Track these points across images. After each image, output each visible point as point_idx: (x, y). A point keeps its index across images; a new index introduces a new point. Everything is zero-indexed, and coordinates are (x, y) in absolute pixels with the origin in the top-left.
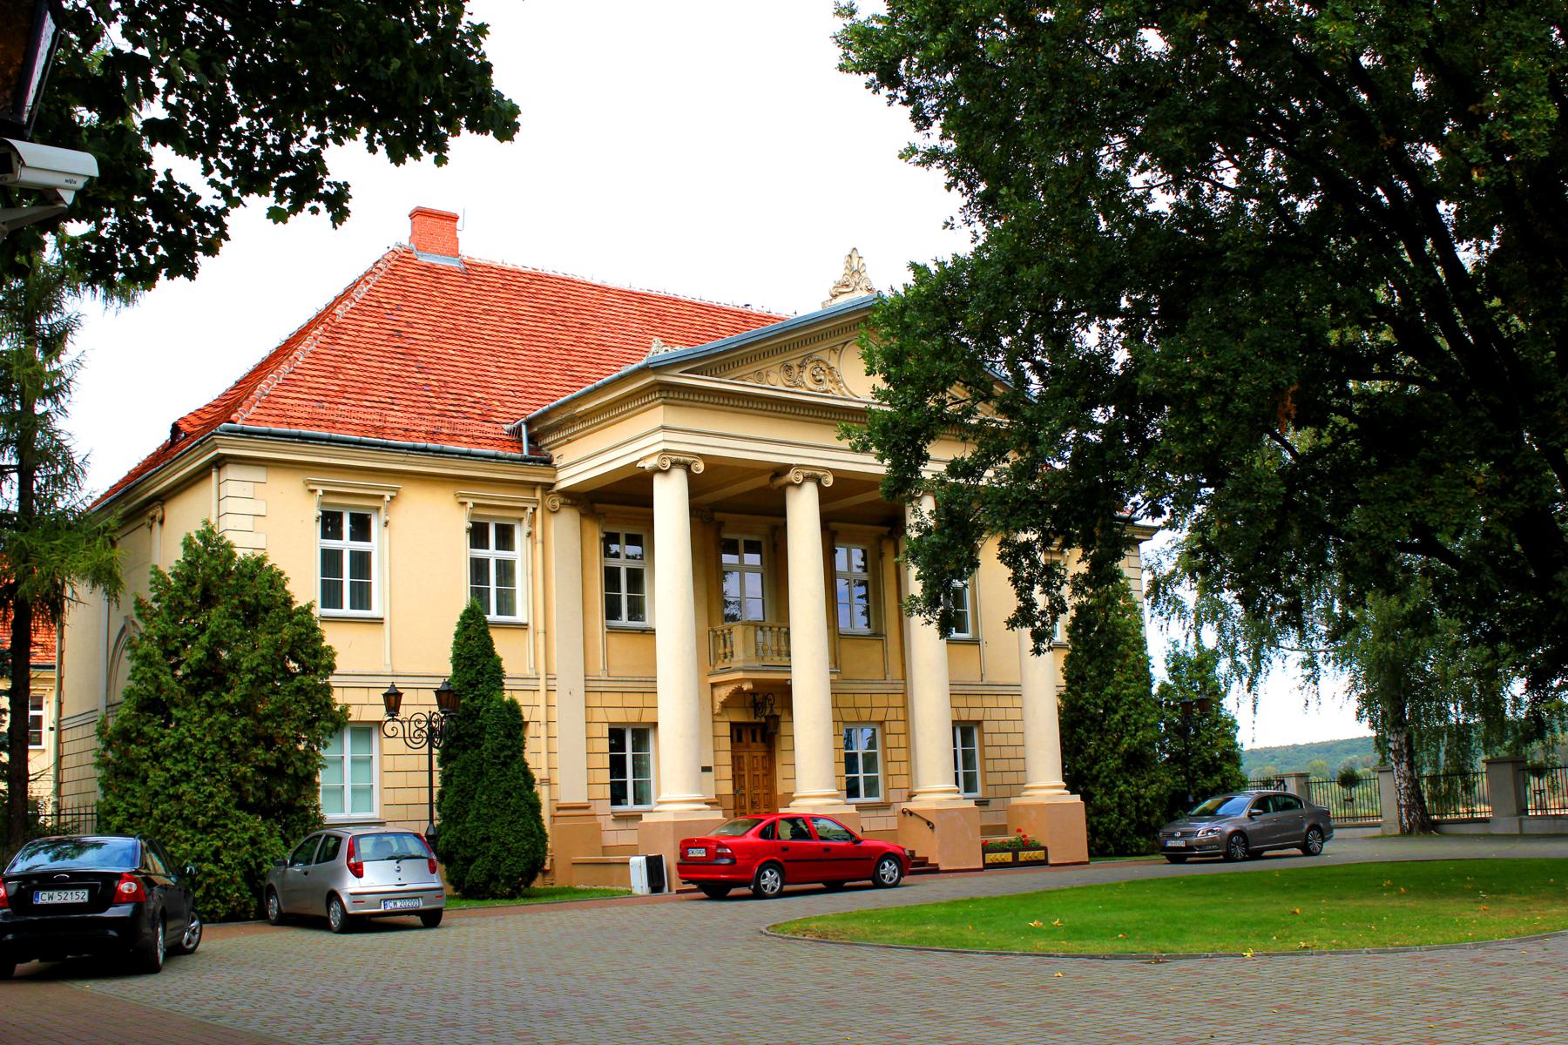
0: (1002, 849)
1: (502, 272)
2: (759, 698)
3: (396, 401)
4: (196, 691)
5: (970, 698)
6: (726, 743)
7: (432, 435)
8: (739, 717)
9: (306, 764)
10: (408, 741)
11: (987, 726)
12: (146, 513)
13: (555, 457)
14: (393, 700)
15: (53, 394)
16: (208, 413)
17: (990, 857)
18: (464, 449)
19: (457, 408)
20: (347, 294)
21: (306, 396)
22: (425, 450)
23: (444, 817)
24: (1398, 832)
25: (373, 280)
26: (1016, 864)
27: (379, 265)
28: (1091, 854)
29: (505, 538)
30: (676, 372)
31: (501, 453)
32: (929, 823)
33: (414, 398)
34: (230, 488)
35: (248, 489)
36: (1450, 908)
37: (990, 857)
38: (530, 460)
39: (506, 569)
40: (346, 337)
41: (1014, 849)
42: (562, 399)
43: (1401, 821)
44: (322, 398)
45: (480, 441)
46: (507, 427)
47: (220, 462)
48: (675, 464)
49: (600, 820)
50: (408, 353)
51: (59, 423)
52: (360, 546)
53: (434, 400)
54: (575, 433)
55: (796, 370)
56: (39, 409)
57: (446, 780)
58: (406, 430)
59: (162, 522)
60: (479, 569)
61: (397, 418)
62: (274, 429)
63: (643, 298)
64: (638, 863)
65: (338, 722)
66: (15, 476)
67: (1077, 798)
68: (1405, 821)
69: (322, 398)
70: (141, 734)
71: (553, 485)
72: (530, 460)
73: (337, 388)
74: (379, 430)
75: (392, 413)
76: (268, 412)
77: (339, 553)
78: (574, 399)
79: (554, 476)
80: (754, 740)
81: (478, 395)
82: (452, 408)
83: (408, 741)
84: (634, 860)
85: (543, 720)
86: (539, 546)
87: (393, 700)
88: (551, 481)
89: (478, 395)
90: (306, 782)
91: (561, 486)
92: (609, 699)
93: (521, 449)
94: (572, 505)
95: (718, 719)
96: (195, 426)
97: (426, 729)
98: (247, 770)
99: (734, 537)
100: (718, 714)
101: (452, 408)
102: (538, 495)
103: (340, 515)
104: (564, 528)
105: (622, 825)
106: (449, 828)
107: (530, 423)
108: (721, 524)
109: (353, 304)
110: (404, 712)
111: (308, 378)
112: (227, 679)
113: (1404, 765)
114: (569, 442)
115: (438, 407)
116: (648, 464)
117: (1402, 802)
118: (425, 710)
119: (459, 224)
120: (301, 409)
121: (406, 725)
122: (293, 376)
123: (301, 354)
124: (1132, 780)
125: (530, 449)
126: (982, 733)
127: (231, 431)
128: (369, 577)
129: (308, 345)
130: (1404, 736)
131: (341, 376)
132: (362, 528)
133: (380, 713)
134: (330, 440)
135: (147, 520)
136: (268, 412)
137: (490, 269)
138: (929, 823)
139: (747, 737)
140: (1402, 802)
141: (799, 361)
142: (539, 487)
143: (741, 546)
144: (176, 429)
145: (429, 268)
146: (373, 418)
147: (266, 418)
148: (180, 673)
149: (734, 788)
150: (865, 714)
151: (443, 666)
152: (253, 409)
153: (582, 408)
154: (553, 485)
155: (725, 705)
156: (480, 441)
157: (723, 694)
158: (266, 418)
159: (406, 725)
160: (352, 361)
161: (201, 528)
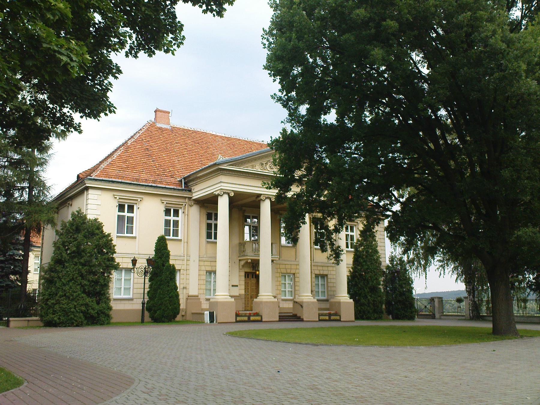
0: (325, 315)
1: (184, 130)
2: (254, 265)
3: (144, 171)
4: (73, 257)
5: (318, 267)
6: (243, 278)
7: (154, 182)
8: (248, 270)
9: (104, 281)
10: (138, 274)
11: (329, 276)
12: (66, 203)
13: (192, 189)
14: (134, 262)
15: (42, 164)
16: (88, 172)
17: (238, 319)
18: (164, 186)
19: (164, 173)
20: (132, 137)
21: (116, 169)
22: (151, 186)
23: (150, 298)
24: (469, 318)
25: (141, 132)
26: (249, 321)
27: (144, 127)
28: (355, 319)
29: (176, 213)
30: (225, 165)
31: (175, 188)
32: (301, 306)
33: (150, 170)
34: (90, 196)
35: (96, 197)
36: (456, 342)
37: (238, 319)
38: (184, 190)
39: (176, 223)
40: (130, 150)
41: (330, 315)
42: (193, 172)
43: (470, 314)
44: (121, 169)
45: (169, 184)
46: (178, 179)
47: (87, 188)
48: (224, 193)
49: (201, 300)
50: (150, 155)
51: (42, 174)
52: (168, 218)
53: (157, 171)
54: (198, 182)
55: (265, 165)
56: (35, 169)
57: (150, 287)
58: (146, 180)
59: (71, 205)
60: (167, 223)
61: (144, 176)
62: (104, 179)
63: (228, 139)
64: (207, 313)
65: (116, 267)
66: (27, 190)
67: (352, 300)
68: (471, 315)
69: (121, 169)
70: (56, 269)
71: (191, 198)
72: (184, 190)
73: (126, 166)
74: (137, 180)
75: (142, 174)
76: (103, 173)
77: (124, 216)
78: (196, 172)
79: (192, 195)
80: (253, 277)
81: (171, 169)
82: (162, 173)
83: (138, 274)
84: (206, 312)
85: (185, 269)
86: (186, 216)
87: (134, 262)
88: (191, 196)
89: (171, 169)
90: (106, 285)
91: (194, 198)
92: (206, 263)
93: (182, 186)
94: (197, 204)
95: (240, 270)
96: (84, 176)
97: (144, 271)
98: (86, 282)
99: (249, 215)
100: (241, 269)
101: (162, 173)
102: (187, 200)
103: (170, 210)
104: (194, 212)
105: (284, 302)
106: (151, 301)
107: (185, 179)
108: (245, 211)
109: (134, 140)
110: (138, 265)
111: (117, 163)
112: (82, 254)
113: (471, 296)
114: (196, 185)
115: (157, 173)
116: (216, 193)
117: (471, 309)
118: (144, 265)
119: (170, 115)
120: (114, 173)
121: (138, 269)
122: (112, 162)
123: (115, 156)
124: (373, 295)
125: (185, 187)
126: (327, 279)
127: (90, 179)
128: (132, 224)
129: (119, 152)
130: (472, 286)
131: (127, 163)
132: (131, 209)
133: (130, 266)
134: (121, 183)
135: (67, 205)
136: (103, 173)
137: (179, 129)
138: (301, 306)
139: (250, 276)
140: (471, 309)
141: (266, 162)
142: (187, 198)
143: (251, 217)
144: (78, 176)
145: (160, 128)
146: (136, 176)
147: (102, 175)
148: (68, 252)
149: (245, 292)
150: (289, 271)
151: (151, 252)
152: (98, 172)
153: (199, 175)
154: (191, 198)
155: (243, 266)
156: (169, 184)
157: (242, 263)
158: (102, 175)
159: (138, 269)
160: (131, 158)
161: (78, 209)
